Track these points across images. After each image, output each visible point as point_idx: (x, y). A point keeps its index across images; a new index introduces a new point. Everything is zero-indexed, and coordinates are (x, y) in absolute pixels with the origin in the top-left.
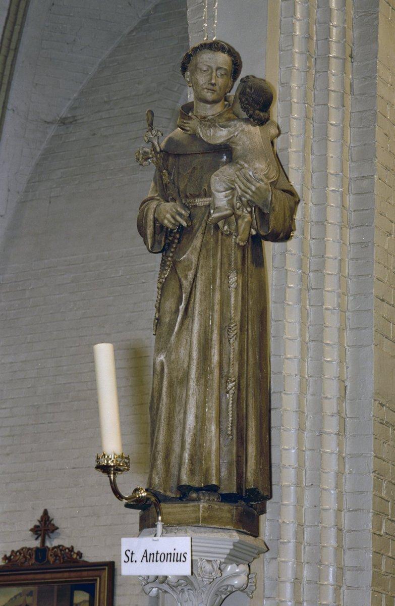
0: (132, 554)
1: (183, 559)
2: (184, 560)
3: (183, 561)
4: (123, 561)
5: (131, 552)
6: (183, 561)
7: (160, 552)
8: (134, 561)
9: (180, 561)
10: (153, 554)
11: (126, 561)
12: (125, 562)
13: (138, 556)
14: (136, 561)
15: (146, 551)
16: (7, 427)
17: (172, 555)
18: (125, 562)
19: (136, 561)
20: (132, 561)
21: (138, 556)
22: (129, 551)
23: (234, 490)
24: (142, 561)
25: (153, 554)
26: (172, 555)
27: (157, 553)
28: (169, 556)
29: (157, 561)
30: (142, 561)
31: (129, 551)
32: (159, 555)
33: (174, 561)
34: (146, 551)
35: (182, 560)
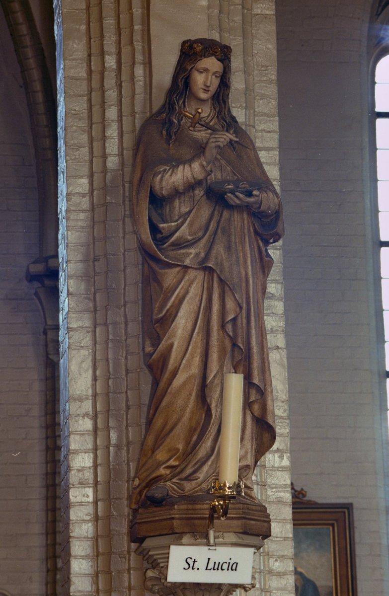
0: (194, 561)
8: (196, 569)
12: (184, 569)
13: (201, 564)
14: (198, 569)
18: (184, 569)
20: (193, 569)
21: (201, 564)
22: (191, 558)
31: (191, 558)
33: (228, 570)
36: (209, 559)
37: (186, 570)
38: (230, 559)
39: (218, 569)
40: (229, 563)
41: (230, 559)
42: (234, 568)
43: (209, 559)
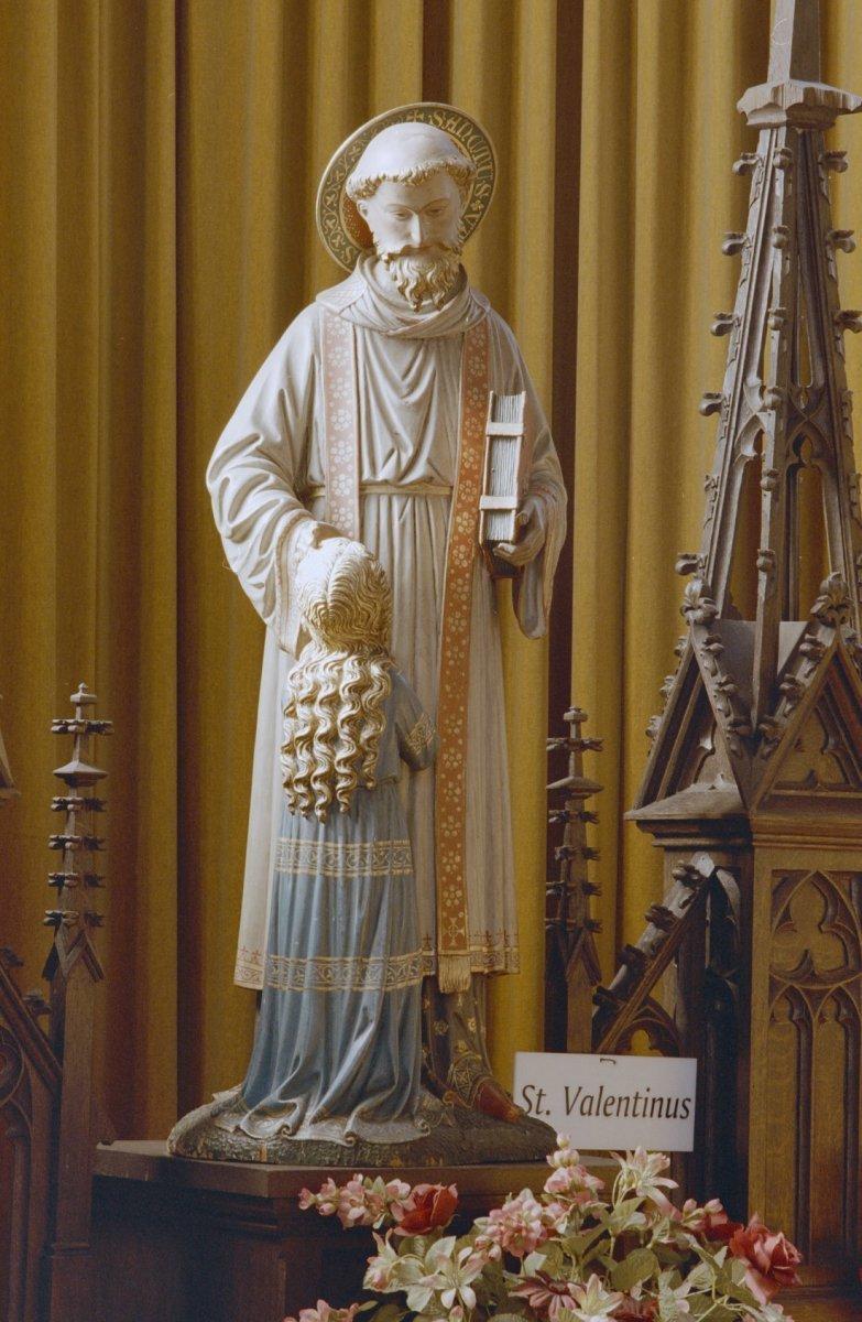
0: (540, 1095)
1: (681, 1111)
2: (684, 1114)
3: (682, 1117)
4: (693, 1100)
5: (537, 1092)
6: (682, 1117)
7: (643, 1094)
9: (675, 1116)
10: (628, 1098)
11: (687, 1102)
14: (548, 1113)
15: (568, 1112)
16: (437, 970)
17: (665, 1102)
19: (548, 1113)
22: (533, 1087)
23: (675, 1076)
24: (580, 1088)
25: (628, 1098)
26: (665, 1102)
27: (636, 1098)
28: (657, 1104)
29: (634, 1115)
30: (580, 1088)
31: (533, 1087)
32: (641, 1103)
33: (644, 1115)
34: (568, 1112)
35: (678, 1114)
36: (567, 1088)
37: (683, 1120)
38: (648, 1090)
39: (590, 1114)
40: (646, 1099)
41: (648, 1090)
42: (586, 1109)
43: (567, 1088)
